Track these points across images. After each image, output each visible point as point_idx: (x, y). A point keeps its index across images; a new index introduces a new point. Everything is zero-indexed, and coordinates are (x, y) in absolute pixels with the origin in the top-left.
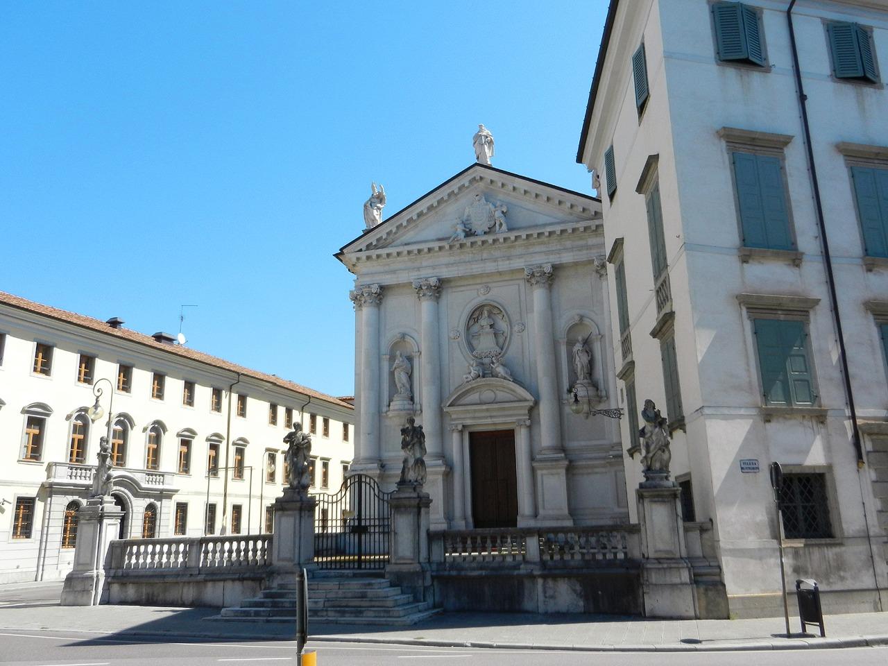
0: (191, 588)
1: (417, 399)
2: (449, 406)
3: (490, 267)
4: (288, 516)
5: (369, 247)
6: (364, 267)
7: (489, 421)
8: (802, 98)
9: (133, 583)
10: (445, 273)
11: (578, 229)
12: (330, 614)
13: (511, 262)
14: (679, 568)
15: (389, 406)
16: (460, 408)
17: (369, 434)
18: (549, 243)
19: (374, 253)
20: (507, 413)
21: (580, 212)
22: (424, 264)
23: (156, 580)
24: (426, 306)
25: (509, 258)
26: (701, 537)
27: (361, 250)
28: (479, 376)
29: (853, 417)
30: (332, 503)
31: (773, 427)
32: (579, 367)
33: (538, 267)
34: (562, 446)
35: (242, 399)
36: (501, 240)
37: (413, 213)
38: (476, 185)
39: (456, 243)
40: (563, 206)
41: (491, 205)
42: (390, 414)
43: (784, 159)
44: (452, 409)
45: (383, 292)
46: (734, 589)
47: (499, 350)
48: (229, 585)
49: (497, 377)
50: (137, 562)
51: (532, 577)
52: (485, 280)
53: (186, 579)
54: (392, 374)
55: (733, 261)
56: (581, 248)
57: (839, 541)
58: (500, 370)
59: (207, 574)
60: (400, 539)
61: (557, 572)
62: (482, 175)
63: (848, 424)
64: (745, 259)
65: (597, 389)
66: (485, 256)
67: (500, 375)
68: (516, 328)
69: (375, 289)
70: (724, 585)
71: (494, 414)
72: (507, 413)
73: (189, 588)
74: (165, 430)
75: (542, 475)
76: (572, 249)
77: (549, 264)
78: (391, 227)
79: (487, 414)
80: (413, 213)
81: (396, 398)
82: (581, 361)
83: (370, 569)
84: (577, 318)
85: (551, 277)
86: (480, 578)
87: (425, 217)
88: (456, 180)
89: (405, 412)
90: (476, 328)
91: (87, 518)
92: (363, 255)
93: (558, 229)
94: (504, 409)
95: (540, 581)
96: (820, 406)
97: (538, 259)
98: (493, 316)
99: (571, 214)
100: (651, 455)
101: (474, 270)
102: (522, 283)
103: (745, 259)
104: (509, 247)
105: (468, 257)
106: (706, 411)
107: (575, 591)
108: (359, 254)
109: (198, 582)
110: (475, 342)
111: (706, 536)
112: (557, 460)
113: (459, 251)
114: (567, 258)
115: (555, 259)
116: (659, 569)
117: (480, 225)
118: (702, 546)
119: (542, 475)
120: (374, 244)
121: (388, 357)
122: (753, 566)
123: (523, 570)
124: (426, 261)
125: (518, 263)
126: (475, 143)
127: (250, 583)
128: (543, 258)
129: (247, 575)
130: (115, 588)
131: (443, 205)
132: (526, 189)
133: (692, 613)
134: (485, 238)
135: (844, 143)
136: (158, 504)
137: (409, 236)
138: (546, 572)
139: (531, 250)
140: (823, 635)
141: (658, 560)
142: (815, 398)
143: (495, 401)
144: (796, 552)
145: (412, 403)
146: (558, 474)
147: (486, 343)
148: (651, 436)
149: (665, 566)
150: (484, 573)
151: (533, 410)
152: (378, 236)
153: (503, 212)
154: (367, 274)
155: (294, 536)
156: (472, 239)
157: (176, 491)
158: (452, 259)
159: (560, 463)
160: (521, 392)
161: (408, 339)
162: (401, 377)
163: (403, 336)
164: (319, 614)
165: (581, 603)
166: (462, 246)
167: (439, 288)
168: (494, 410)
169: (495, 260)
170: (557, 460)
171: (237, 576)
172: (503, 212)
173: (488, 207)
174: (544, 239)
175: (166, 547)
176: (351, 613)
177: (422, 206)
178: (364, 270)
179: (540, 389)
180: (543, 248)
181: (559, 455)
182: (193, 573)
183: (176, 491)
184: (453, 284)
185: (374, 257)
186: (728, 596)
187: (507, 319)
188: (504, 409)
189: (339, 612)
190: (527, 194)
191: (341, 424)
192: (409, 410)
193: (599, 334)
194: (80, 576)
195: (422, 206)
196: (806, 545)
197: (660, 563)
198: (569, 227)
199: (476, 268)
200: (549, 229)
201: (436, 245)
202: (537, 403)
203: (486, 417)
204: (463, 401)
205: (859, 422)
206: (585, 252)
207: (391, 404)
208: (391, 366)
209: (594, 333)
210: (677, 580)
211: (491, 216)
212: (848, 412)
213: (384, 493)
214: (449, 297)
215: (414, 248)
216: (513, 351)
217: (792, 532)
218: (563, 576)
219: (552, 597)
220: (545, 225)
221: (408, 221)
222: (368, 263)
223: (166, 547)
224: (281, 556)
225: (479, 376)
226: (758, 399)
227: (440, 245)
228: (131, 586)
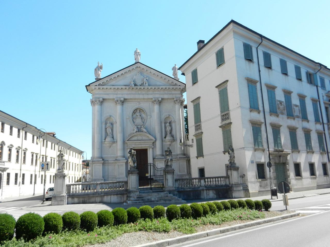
0: (99, 198)
1: (115, 138)
2: (127, 141)
3: (141, 97)
4: (134, 175)
5: (99, 85)
6: (97, 92)
7: (140, 146)
8: (260, 71)
9: (77, 197)
10: (126, 97)
11: (170, 88)
12: (162, 201)
13: (149, 96)
14: (240, 186)
15: (105, 139)
16: (131, 142)
17: (99, 149)
18: (160, 91)
19: (101, 87)
20: (146, 144)
21: (171, 83)
22: (119, 93)
23: (86, 196)
24: (119, 107)
25: (148, 94)
26: (242, 179)
27: (96, 85)
28: (137, 132)
29: (269, 151)
30: (160, 171)
31: (256, 152)
32: (168, 131)
33: (157, 98)
34: (163, 154)
35: (26, 133)
36: (146, 88)
37: (116, 75)
38: (137, 69)
39: (131, 87)
40: (165, 80)
41: (142, 76)
42: (106, 142)
43: (275, 92)
44: (128, 142)
45: (102, 102)
46: (251, 191)
47: (143, 124)
48: (112, 196)
49: (143, 132)
50: (211, 184)
51: (203, 190)
52: (138, 100)
53: (97, 195)
54: (106, 129)
55: (248, 111)
56: (170, 94)
57: (266, 179)
58: (144, 130)
59: (104, 193)
60: (169, 181)
61: (209, 188)
62: (140, 66)
63: (268, 152)
64: (251, 111)
65: (173, 138)
66: (139, 93)
67: (144, 131)
68: (149, 117)
69: (101, 100)
70: (249, 190)
71: (143, 144)
72: (146, 144)
73: (98, 199)
74: (4, 144)
75: (157, 163)
76: (167, 94)
77: (161, 98)
78: (108, 79)
79: (140, 144)
80: (116, 75)
81: (108, 137)
82: (168, 129)
83: (156, 190)
84: (168, 115)
85: (160, 102)
86: (190, 191)
87: (119, 77)
88: (132, 66)
89: (112, 142)
90: (135, 116)
91: (59, 177)
92: (97, 87)
93: (164, 87)
94: (145, 142)
95: (205, 191)
96: (263, 148)
97: (157, 96)
98: (140, 112)
99: (167, 83)
100: (231, 159)
101: (136, 97)
102: (151, 103)
103: (251, 111)
104: (148, 91)
105: (134, 92)
106: (245, 148)
107: (214, 193)
108: (96, 87)
109: (101, 196)
110: (134, 120)
111: (243, 178)
112: (162, 159)
113: (131, 90)
114: (166, 97)
115: (162, 96)
116: (236, 187)
117: (139, 83)
118: (242, 181)
119: (157, 163)
120: (101, 84)
121: (105, 123)
122: (253, 185)
123: (201, 188)
124: (119, 92)
125: (151, 96)
126: (135, 54)
127: (120, 195)
128: (158, 96)
129: (119, 193)
130: (70, 199)
131: (126, 74)
132: (154, 73)
133: (243, 197)
134: (141, 87)
135: (248, 78)
136: (2, 173)
137: (113, 83)
138: (207, 189)
139: (155, 93)
140: (277, 198)
141: (235, 184)
142: (262, 146)
143: (142, 140)
144: (260, 182)
145: (113, 139)
146: (162, 163)
147: (138, 121)
148: (231, 154)
149: (237, 186)
150: (191, 189)
151: (154, 143)
152: (103, 81)
153: (146, 79)
154: (97, 94)
155: (136, 181)
156: (137, 87)
157: (8, 168)
158: (129, 92)
159: (163, 159)
160: (151, 137)
161: (112, 117)
162: (109, 130)
163: (110, 116)
164: (159, 201)
165: (215, 196)
166: (133, 88)
167: (123, 102)
168: (142, 143)
169: (143, 94)
170: (162, 159)
171: (116, 194)
172: (146, 79)
173: (141, 77)
174: (159, 90)
175: (212, 180)
176: (168, 201)
177: (119, 73)
178: (97, 92)
179: (156, 136)
180: (159, 93)
181: (163, 157)
182: (99, 193)
183: (8, 168)
184: (127, 101)
185: (101, 88)
186: (250, 192)
187: (146, 113)
188: (145, 142)
189: (164, 200)
190: (154, 75)
191: (51, 143)
192: (112, 141)
193: (174, 121)
194: (59, 196)
195: (119, 73)
196: (262, 180)
197: (235, 185)
198: (168, 87)
199: (137, 96)
200: (162, 87)
201: (124, 87)
202: (156, 141)
203: (139, 145)
204: (131, 139)
205: (270, 152)
206: (171, 95)
207: (106, 139)
208: (105, 126)
209: (172, 120)
210: (240, 189)
211: (143, 80)
212: (268, 150)
213: (158, 169)
214: (126, 105)
215: (116, 87)
216: (147, 124)
217: (259, 178)
218: (211, 189)
219: (208, 195)
220: (160, 85)
221: (114, 78)
222: (99, 90)
223: (212, 180)
224: (132, 187)
225: (137, 132)
226: (253, 146)
227: (126, 87)
228: (76, 198)
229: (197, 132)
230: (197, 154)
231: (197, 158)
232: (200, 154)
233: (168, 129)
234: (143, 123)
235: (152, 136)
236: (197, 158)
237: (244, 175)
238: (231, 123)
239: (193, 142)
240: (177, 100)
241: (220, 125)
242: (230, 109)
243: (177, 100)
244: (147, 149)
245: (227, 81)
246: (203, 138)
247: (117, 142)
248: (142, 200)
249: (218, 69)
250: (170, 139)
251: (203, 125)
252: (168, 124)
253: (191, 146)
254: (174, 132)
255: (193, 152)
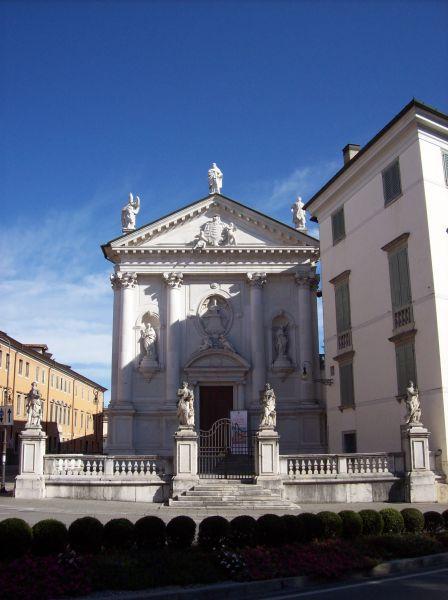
7: (215, 379)
32: (280, 346)
82: (281, 342)
151: (248, 373)
188: (227, 372)
202: (251, 369)
229: (400, 330)
230: (342, 402)
231: (342, 411)
232: (348, 400)
233: (281, 342)
234: (225, 328)
235: (244, 358)
236: (342, 411)
237: (440, 450)
238: (414, 331)
239: (333, 373)
240: (301, 279)
241: (391, 335)
242: (352, 325)
243: (301, 279)
244: (232, 387)
245: (406, 235)
246: (354, 365)
247: (165, 368)
248: (201, 499)
249: (387, 209)
250: (284, 365)
251: (355, 336)
252: (280, 332)
253: (330, 382)
254: (293, 352)
255: (333, 395)
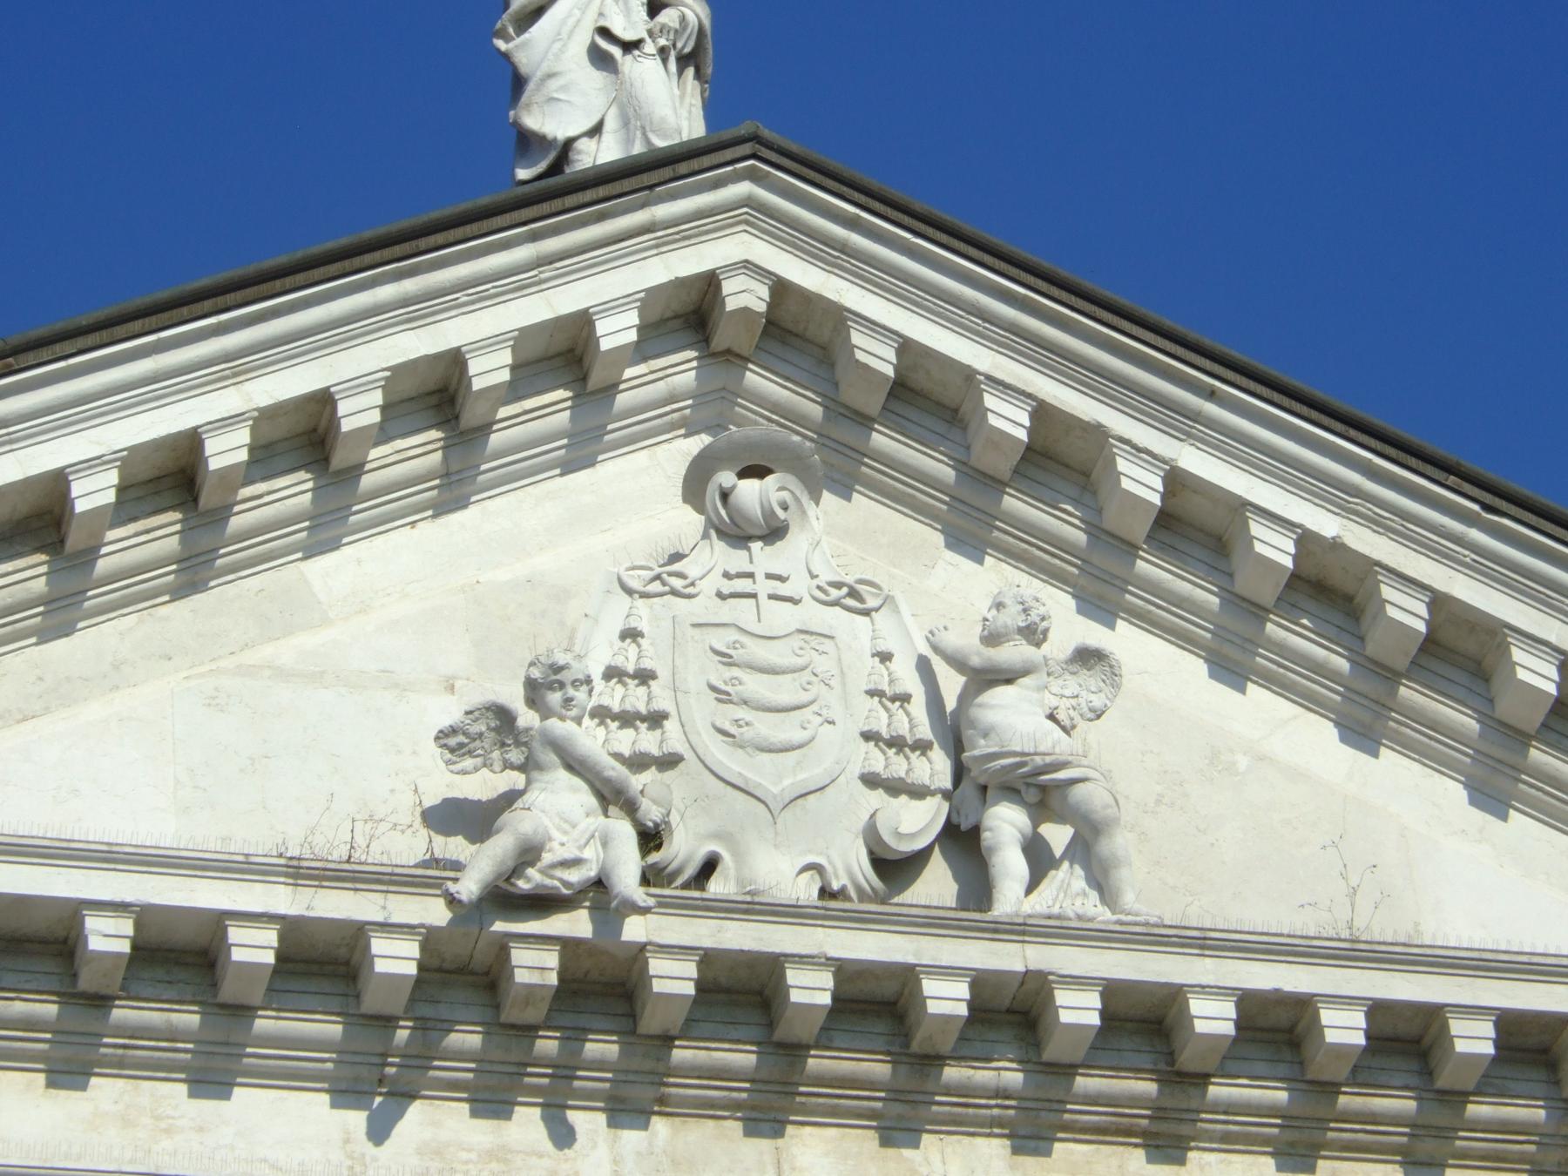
82: (558, 45)
